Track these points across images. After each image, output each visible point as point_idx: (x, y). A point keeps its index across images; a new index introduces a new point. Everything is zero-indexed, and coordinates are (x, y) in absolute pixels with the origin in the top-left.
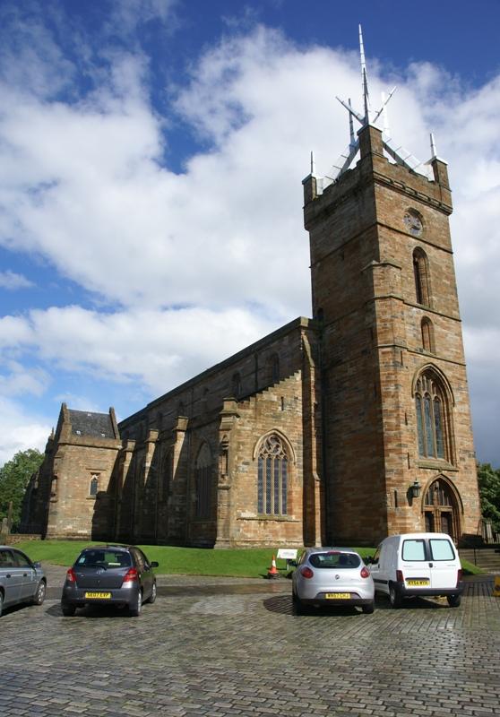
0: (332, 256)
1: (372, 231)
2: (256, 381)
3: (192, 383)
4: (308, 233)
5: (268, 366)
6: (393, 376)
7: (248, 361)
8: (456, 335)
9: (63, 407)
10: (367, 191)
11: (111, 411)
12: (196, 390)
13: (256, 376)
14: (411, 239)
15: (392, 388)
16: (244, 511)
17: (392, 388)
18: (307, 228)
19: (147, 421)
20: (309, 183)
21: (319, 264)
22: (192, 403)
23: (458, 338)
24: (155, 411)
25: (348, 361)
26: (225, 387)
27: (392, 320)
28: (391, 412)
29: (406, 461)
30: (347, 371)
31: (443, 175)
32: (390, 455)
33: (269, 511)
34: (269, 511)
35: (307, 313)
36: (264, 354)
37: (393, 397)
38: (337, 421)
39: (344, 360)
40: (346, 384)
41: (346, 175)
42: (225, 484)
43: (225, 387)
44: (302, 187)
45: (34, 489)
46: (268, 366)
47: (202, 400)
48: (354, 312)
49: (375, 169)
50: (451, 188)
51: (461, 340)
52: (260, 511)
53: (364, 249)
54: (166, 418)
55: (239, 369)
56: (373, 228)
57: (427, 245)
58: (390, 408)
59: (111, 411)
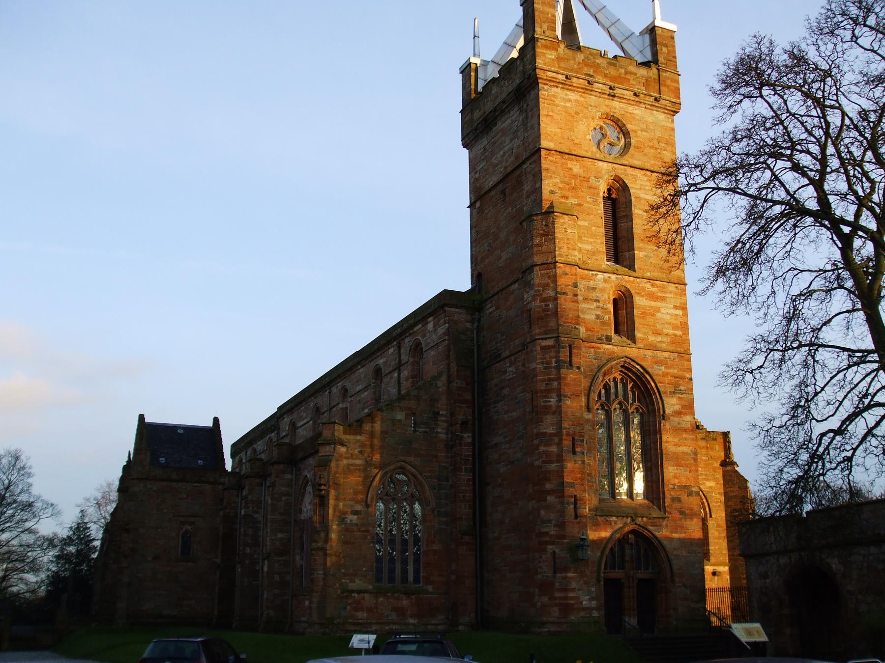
0: (493, 193)
1: (535, 161)
2: (399, 382)
3: (288, 407)
4: (466, 152)
5: (411, 360)
6: (556, 383)
7: (391, 351)
8: (675, 307)
9: (142, 418)
10: (533, 93)
11: (216, 421)
12: (335, 390)
13: (399, 374)
14: (601, 163)
15: (553, 400)
16: (352, 581)
17: (553, 400)
18: (465, 145)
19: (278, 434)
20: (467, 70)
21: (478, 204)
22: (331, 409)
23: (680, 312)
24: (287, 419)
25: (506, 358)
26: (365, 389)
27: (556, 299)
28: (552, 435)
29: (572, 507)
30: (505, 372)
31: (665, 49)
32: (549, 498)
33: (391, 580)
34: (391, 580)
35: (462, 283)
36: (408, 342)
37: (554, 413)
38: (496, 444)
39: (504, 355)
40: (506, 391)
41: (508, 68)
42: (320, 544)
43: (365, 389)
44: (460, 77)
45: (439, 412)
46: (411, 360)
47: (341, 406)
48: (514, 282)
49: (539, 63)
50: (680, 69)
51: (685, 315)
52: (379, 579)
53: (527, 187)
54: (300, 430)
55: (381, 361)
56: (535, 158)
57: (630, 171)
58: (550, 430)
59: (216, 421)
